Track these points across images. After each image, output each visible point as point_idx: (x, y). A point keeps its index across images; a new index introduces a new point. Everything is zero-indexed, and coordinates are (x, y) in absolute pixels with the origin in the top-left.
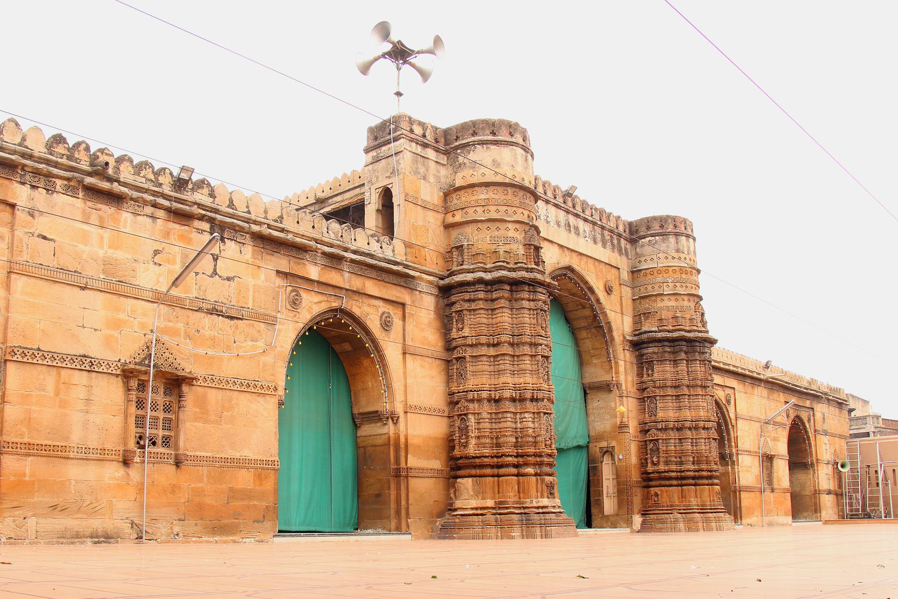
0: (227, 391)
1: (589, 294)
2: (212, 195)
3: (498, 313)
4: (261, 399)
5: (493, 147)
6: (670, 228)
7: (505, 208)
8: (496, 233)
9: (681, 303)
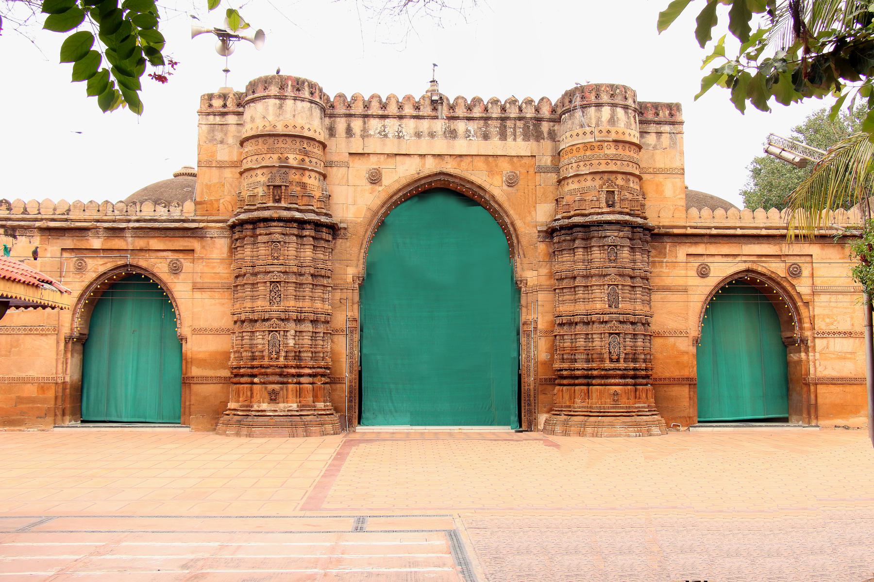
0: (15, 335)
2: (9, 209)
4: (44, 338)
5: (252, 105)
6: (605, 98)
7: (256, 157)
8: (251, 180)
9: (584, 184)
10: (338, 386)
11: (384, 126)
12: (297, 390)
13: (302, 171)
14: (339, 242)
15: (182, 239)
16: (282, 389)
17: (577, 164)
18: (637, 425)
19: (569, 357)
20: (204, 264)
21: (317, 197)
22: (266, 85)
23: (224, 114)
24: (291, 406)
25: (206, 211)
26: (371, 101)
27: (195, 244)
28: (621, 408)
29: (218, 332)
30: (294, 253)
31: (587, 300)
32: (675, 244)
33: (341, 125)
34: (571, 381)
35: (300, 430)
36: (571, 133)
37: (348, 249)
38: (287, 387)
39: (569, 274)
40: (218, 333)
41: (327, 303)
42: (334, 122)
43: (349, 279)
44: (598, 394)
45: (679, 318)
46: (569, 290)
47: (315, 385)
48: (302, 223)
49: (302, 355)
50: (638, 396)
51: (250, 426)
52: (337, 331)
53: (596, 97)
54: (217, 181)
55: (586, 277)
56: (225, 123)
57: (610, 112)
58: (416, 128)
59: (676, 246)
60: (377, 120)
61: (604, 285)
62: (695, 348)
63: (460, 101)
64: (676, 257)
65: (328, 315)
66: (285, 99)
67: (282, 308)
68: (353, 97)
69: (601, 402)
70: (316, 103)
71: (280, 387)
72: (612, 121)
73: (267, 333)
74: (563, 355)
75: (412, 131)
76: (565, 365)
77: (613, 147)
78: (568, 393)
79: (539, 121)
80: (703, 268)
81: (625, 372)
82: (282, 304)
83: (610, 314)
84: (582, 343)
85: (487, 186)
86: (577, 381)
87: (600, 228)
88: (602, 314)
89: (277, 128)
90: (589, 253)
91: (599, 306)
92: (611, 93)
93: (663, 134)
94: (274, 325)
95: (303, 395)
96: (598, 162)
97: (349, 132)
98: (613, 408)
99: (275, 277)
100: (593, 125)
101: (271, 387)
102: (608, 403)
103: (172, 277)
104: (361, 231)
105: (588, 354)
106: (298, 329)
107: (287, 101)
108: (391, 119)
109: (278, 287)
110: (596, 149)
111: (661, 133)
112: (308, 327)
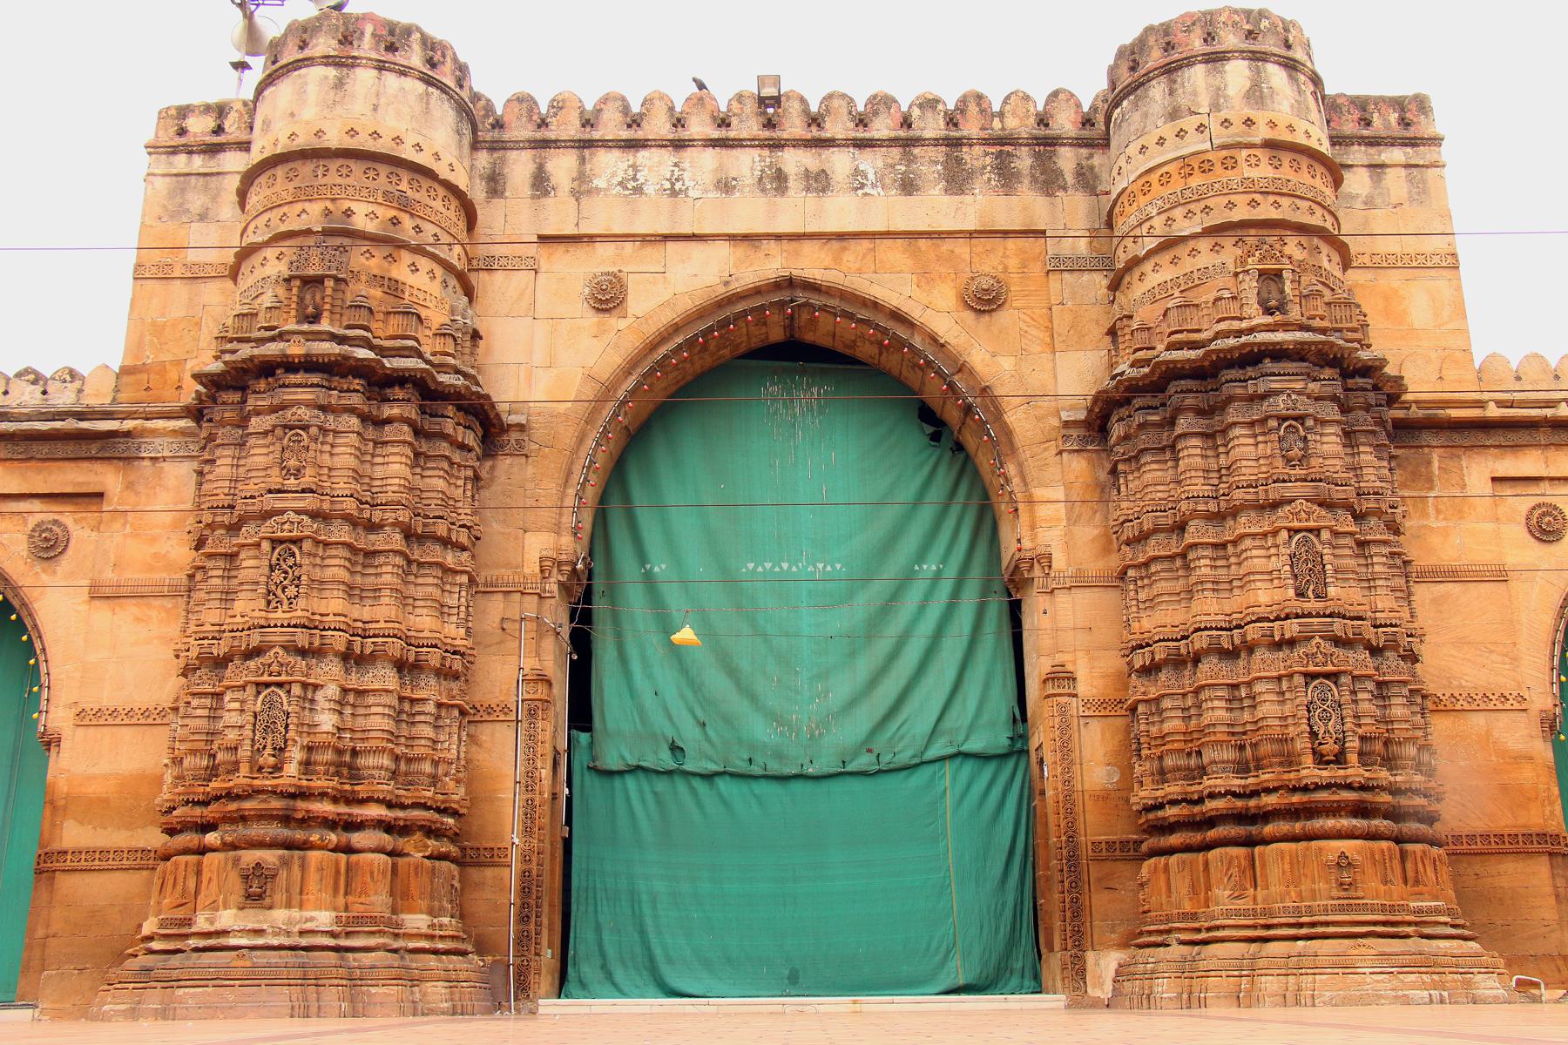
1: (902, 332)
3: (392, 454)
7: (265, 217)
9: (1188, 264)
10: (489, 873)
11: (635, 167)
12: (338, 872)
13: (386, 250)
14: (504, 464)
15: (73, 464)
16: (285, 863)
17: (1164, 217)
18: (1427, 964)
19: (1181, 762)
20: (128, 529)
21: (435, 326)
22: (305, 36)
23: (213, 150)
24: (312, 919)
25: (148, 389)
26: (600, 110)
27: (107, 478)
28: (1365, 908)
29: (148, 718)
30: (352, 462)
31: (1227, 586)
32: (1454, 451)
33: (520, 166)
34: (1195, 837)
35: (331, 995)
36: (1141, 142)
37: (530, 486)
38: (303, 859)
39: (1167, 520)
40: (150, 721)
41: (454, 619)
42: (503, 161)
43: (532, 567)
44: (1287, 867)
45: (1494, 657)
46: (1166, 565)
47: (401, 861)
48: (380, 382)
49: (362, 761)
50: (1410, 874)
51: (170, 983)
52: (490, 710)
53: (1205, 40)
54: (183, 313)
55: (1218, 517)
56: (214, 170)
57: (1247, 72)
58: (720, 168)
59: (1459, 457)
60: (616, 154)
61: (1275, 533)
62: (1549, 745)
63: (836, 103)
64: (1464, 487)
65: (455, 653)
66: (353, 66)
67: (299, 613)
68: (553, 100)
69: (1300, 895)
70: (443, 88)
71: (281, 857)
72: (1256, 94)
73: (251, 690)
74: (1161, 758)
75: (708, 178)
76: (1173, 789)
77: (1264, 160)
78: (1186, 872)
79: (1050, 145)
80: (1544, 514)
81: (1367, 796)
82: (302, 603)
83: (1303, 616)
84: (1222, 713)
85: (915, 312)
86: (1212, 834)
87: (1250, 372)
88: (1278, 618)
89: (325, 138)
90: (1221, 449)
91: (1264, 596)
92: (1248, 27)
93: (1388, 170)
94: (275, 668)
95: (357, 885)
96: (1225, 200)
97: (541, 183)
98: (1342, 909)
99: (286, 526)
100: (1204, 109)
101: (250, 857)
102: (1322, 894)
103: (38, 569)
104: (568, 436)
105: (1242, 748)
106: (354, 681)
107: (358, 70)
108: (653, 150)
109: (293, 555)
110: (1218, 168)
111: (1383, 166)
112: (383, 677)
